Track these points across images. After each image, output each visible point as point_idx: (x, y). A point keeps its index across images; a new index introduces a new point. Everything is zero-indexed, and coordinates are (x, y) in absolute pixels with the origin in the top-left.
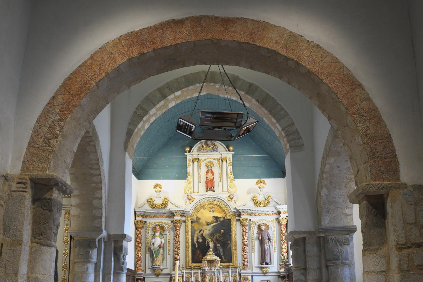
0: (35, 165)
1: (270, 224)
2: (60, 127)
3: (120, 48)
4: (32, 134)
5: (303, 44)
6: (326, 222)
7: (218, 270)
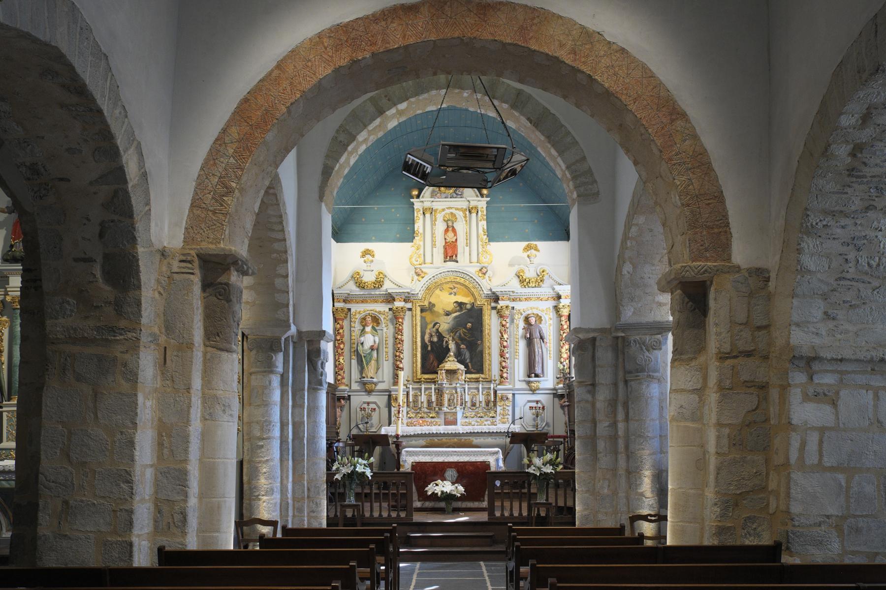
0: (203, 234)
1: (544, 314)
2: (237, 177)
3: (322, 51)
4: (196, 188)
5: (600, 48)
6: (628, 315)
7: (462, 384)
